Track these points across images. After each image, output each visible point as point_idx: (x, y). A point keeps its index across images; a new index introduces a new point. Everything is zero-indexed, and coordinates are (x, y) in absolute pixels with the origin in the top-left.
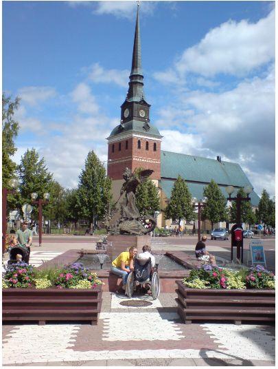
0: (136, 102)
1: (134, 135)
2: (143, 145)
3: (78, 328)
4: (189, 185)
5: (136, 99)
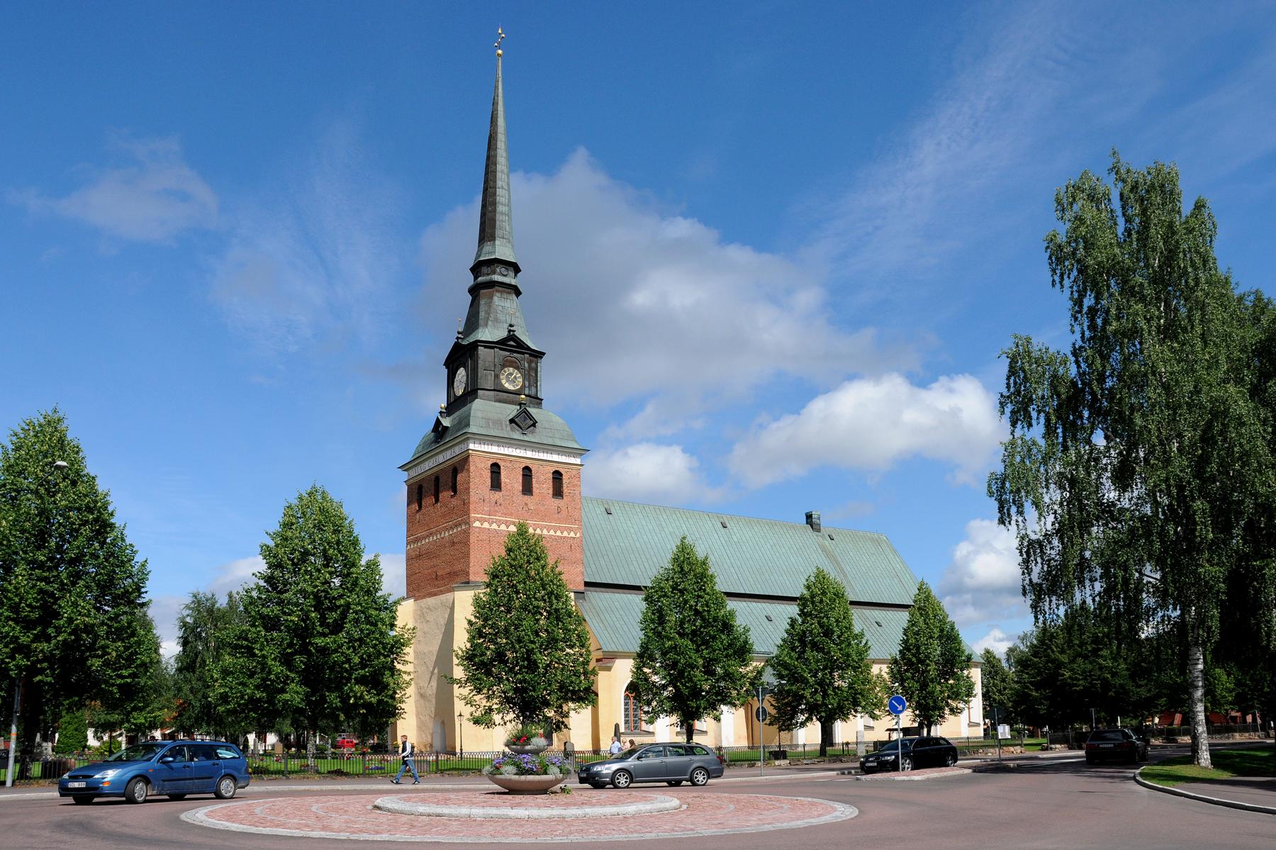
0: (489, 345)
1: (471, 446)
2: (512, 480)
3: (675, 802)
4: (731, 604)
5: (489, 333)
